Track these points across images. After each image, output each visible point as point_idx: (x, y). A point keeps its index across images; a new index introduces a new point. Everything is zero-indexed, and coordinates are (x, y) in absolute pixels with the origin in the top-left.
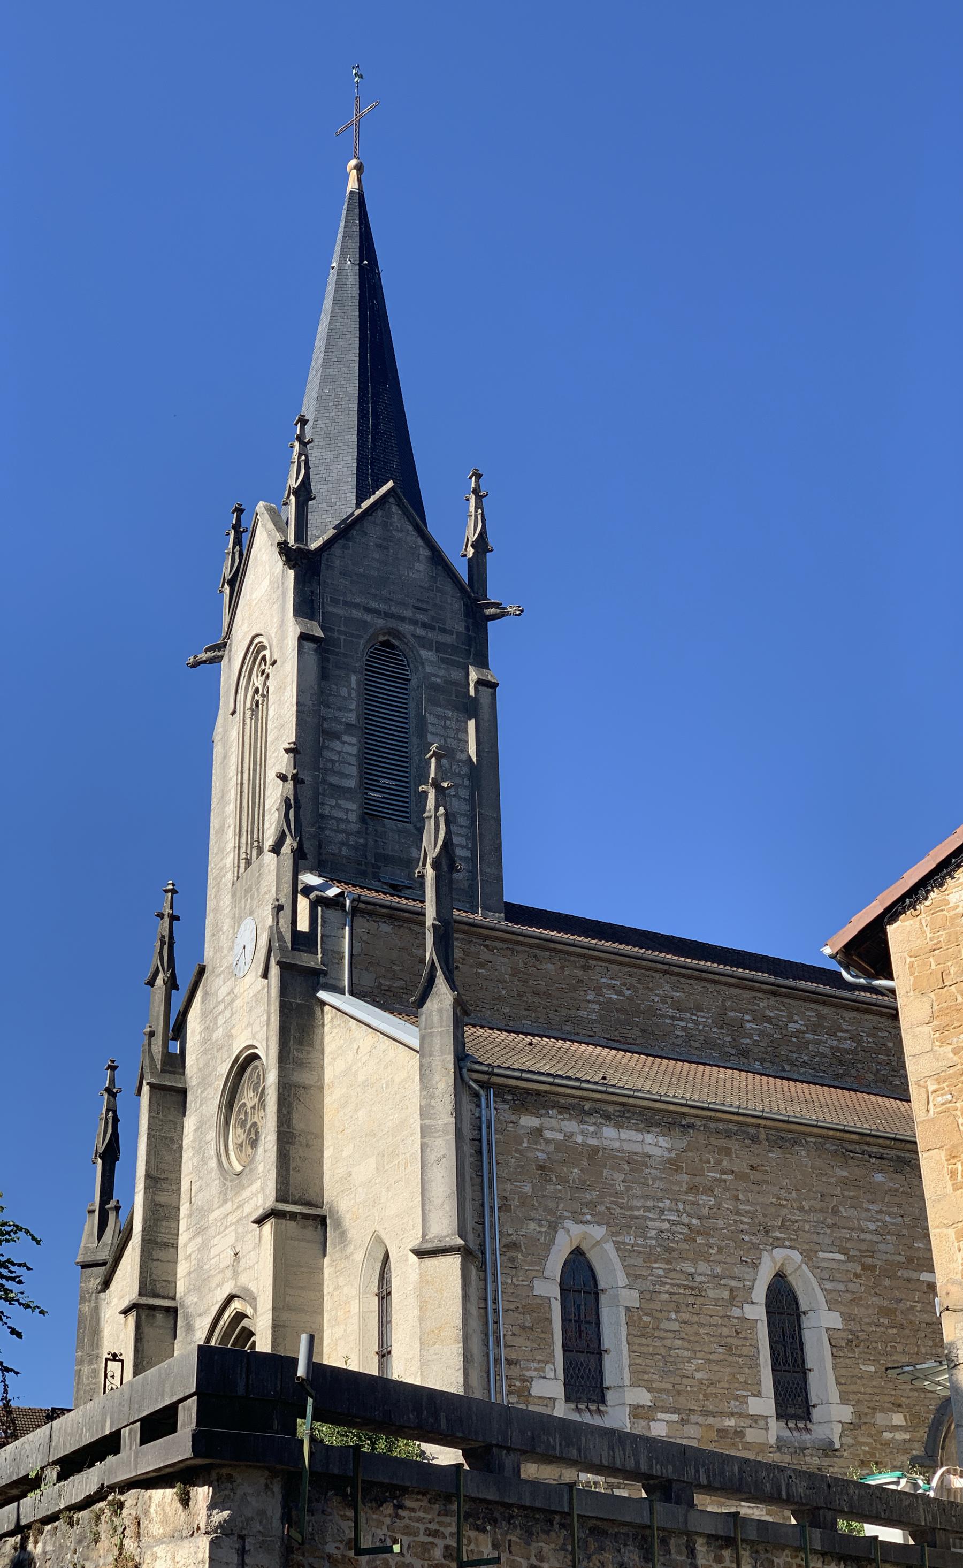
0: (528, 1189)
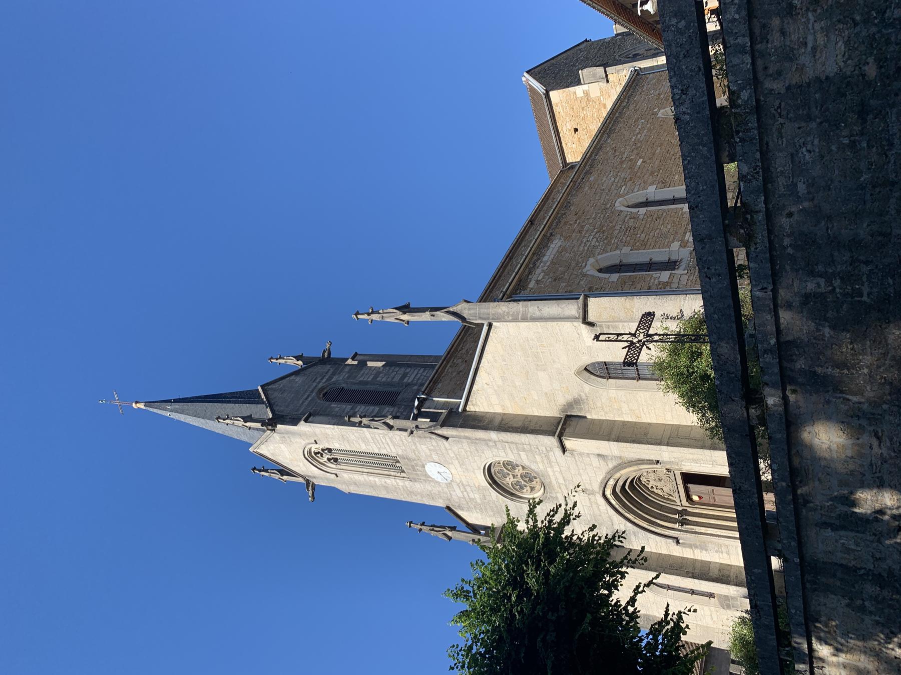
0: (564, 284)
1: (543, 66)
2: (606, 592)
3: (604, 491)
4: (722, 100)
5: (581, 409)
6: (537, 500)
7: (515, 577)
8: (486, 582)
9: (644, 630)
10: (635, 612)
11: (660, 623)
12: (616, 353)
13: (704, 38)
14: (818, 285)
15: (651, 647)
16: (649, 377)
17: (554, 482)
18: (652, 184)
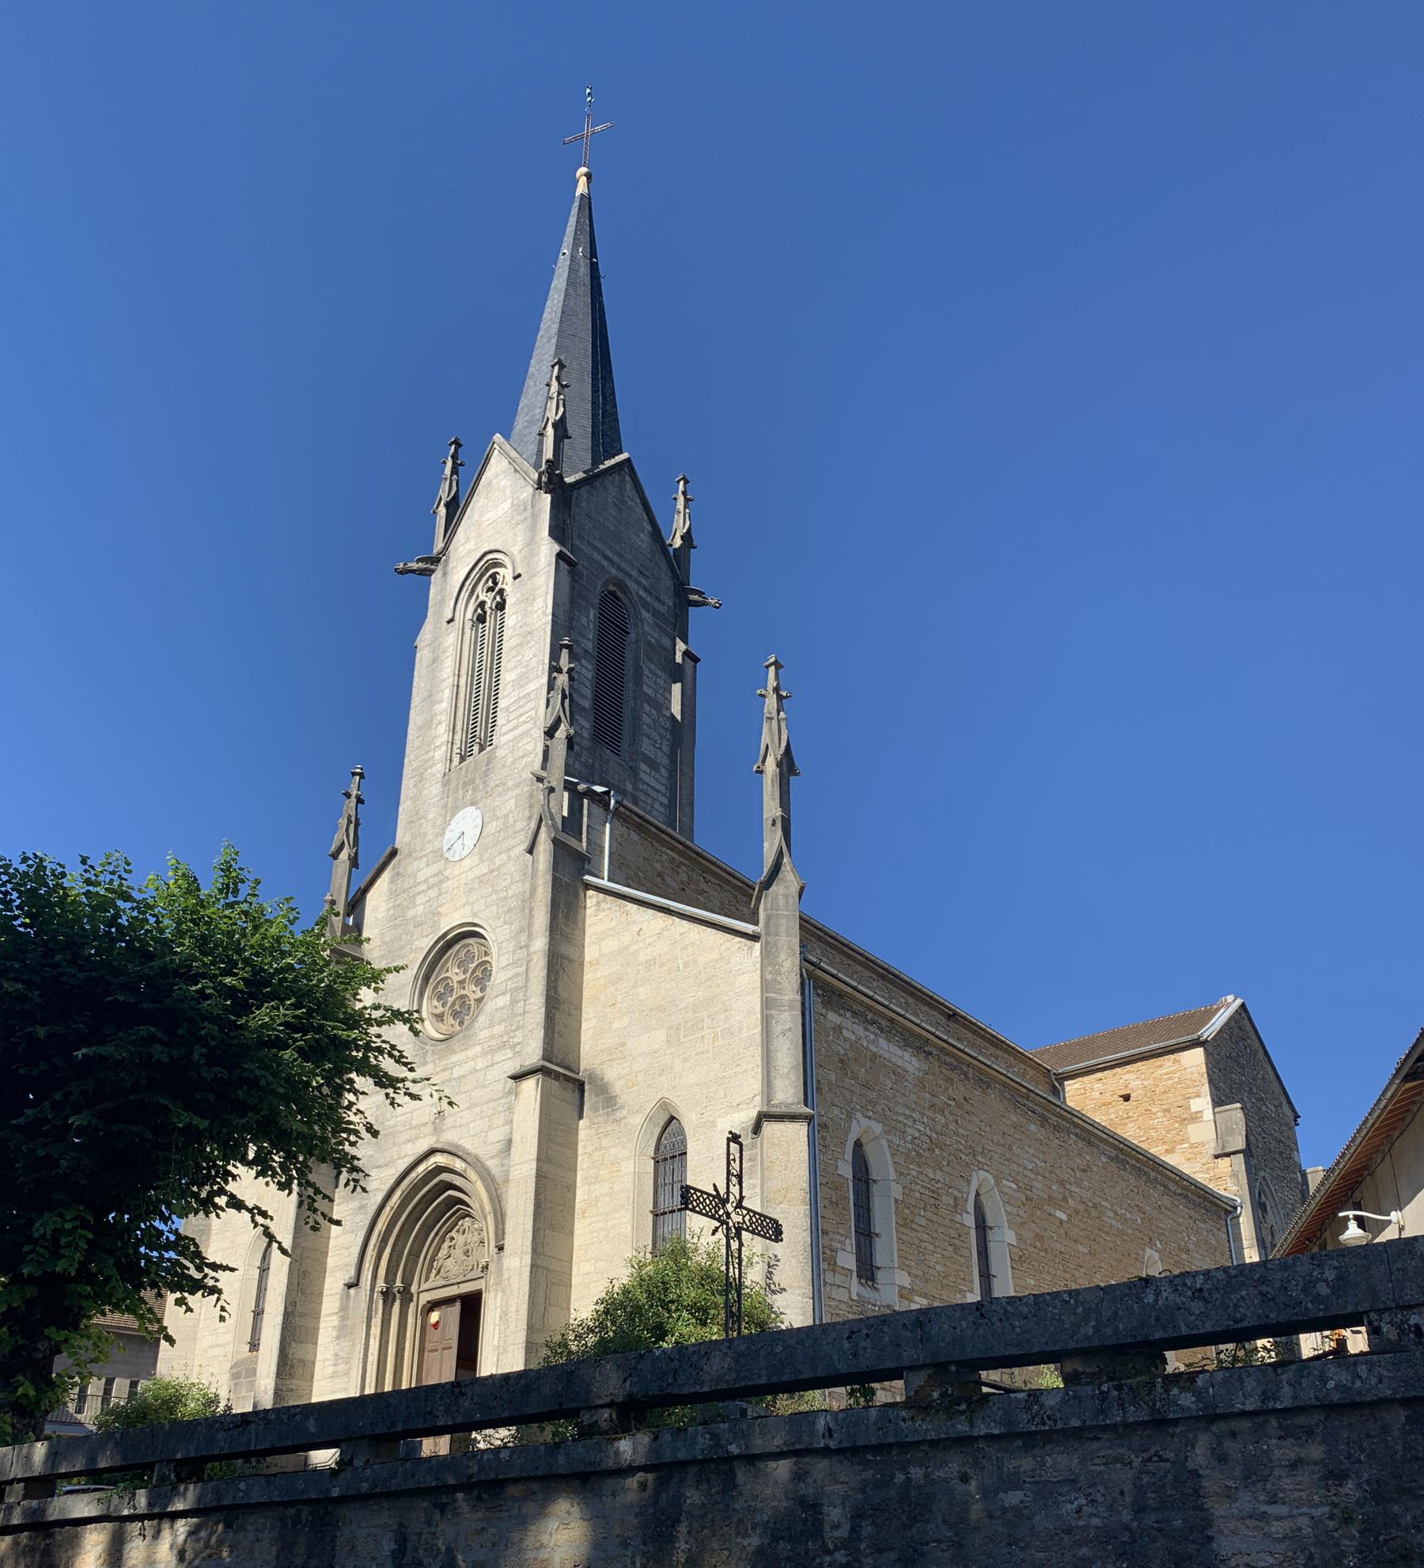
0: (833, 1078)
1: (1252, 1035)
2: (251, 1155)
3: (442, 1151)
4: (1176, 1361)
5: (597, 1110)
6: (418, 1026)
7: (269, 984)
8: (256, 928)
9: (189, 1226)
10: (216, 1207)
11: (198, 1254)
12: (705, 1170)
13: (1286, 1330)
14: (836, 1527)
15: (154, 1239)
16: (660, 1232)
17: (454, 1058)
18: (1019, 1238)
